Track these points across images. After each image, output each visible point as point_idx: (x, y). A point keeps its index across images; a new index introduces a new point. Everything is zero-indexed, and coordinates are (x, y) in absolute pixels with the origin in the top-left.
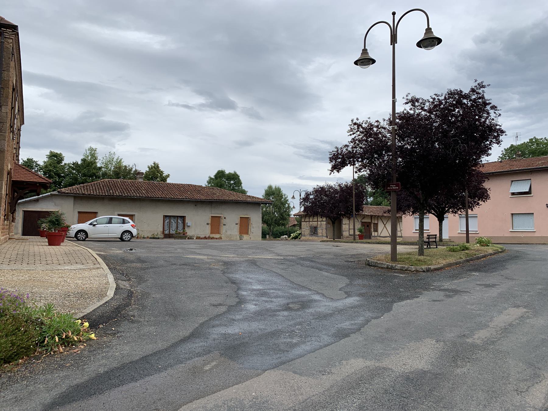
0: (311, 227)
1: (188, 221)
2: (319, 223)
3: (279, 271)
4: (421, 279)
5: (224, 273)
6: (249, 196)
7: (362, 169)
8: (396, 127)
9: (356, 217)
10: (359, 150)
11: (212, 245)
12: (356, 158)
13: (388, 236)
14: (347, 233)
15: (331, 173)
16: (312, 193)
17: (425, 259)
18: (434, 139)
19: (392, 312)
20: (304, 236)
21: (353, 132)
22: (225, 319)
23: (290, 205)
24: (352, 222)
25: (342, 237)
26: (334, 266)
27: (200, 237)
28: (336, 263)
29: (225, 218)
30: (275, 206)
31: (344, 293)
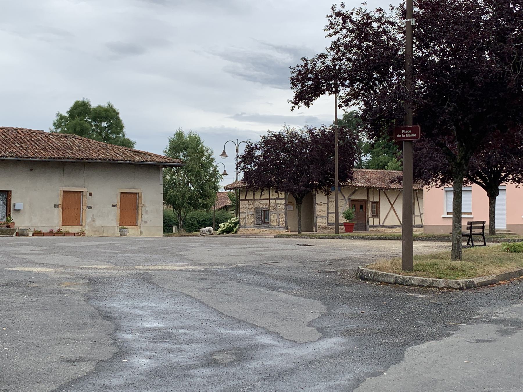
0: (257, 211)
1: (16, 201)
2: (273, 202)
3: (195, 293)
4: (456, 303)
5: (89, 298)
6: (138, 152)
7: (350, 101)
8: (413, 22)
9: (340, 190)
10: (345, 65)
11: (65, 246)
12: (339, 80)
13: (399, 226)
14: (325, 220)
15: (293, 107)
16: (259, 146)
17: (464, 265)
18: (483, 44)
19: (403, 363)
20: (244, 227)
21: (334, 30)
22: (90, 386)
23: (218, 169)
24: (332, 200)
25: (314, 228)
26: (298, 281)
27: (41, 231)
28: (302, 276)
29: (91, 194)
30: (189, 171)
31: (316, 331)
